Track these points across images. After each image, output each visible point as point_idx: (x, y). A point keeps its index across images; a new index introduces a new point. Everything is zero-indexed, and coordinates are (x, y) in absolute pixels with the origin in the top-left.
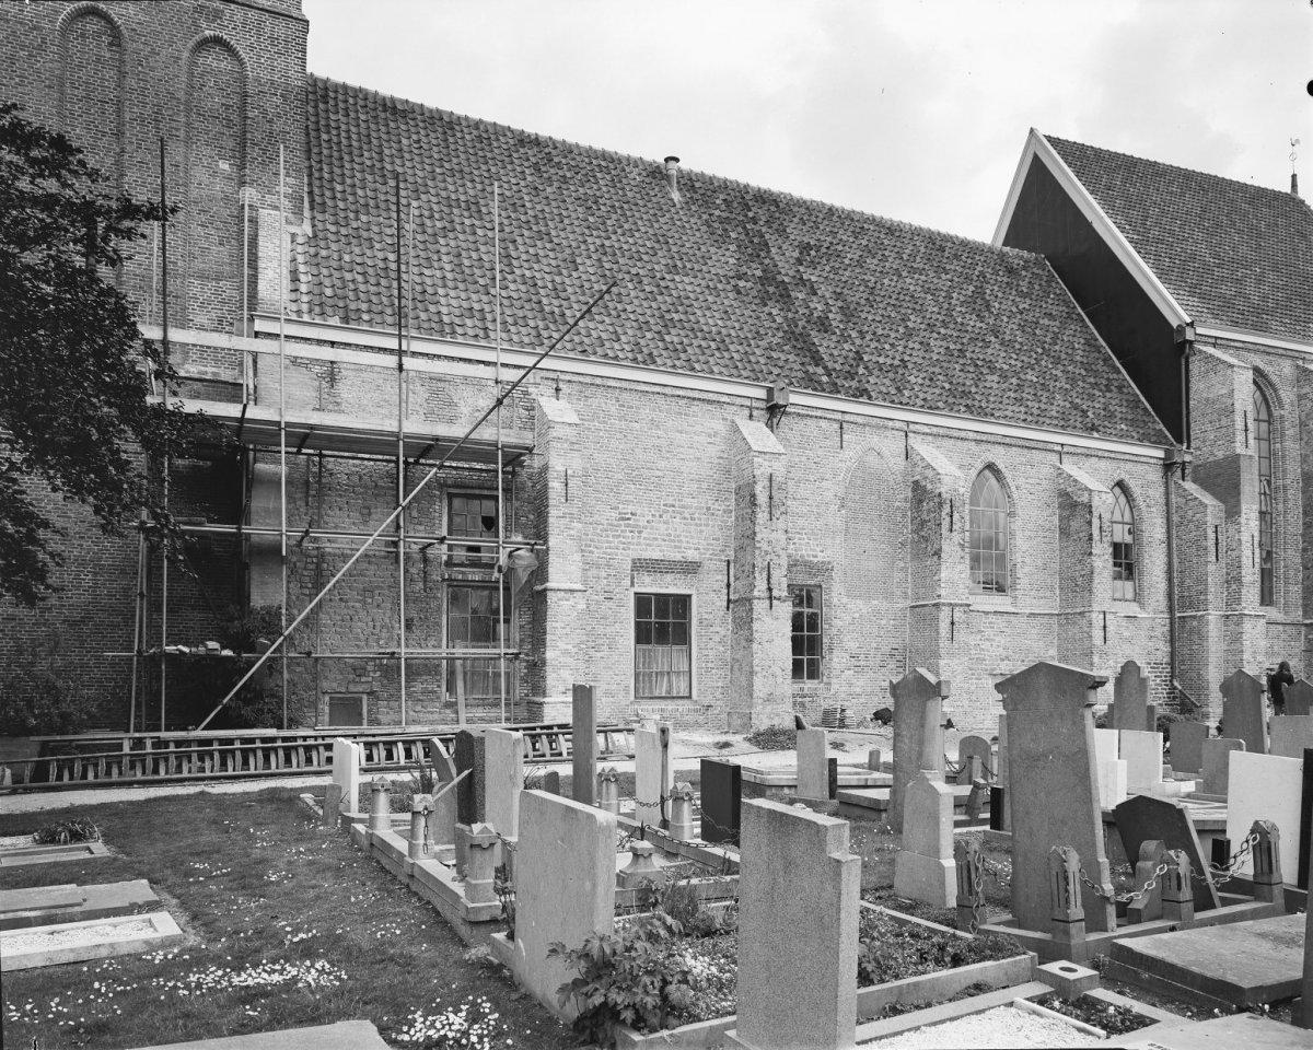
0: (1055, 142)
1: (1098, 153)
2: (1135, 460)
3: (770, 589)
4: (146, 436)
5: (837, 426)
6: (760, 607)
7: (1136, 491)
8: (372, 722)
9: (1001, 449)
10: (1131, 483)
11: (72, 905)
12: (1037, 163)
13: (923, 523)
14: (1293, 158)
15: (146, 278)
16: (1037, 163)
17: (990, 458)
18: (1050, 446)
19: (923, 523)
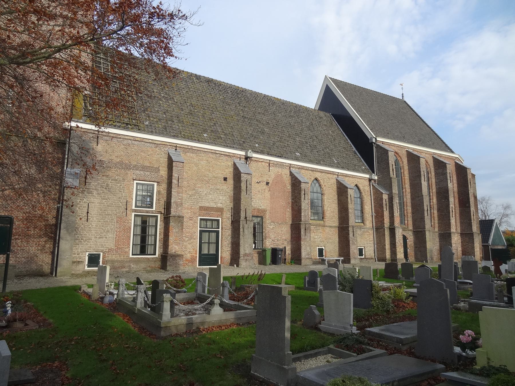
5: (268, 165)
7: (361, 188)
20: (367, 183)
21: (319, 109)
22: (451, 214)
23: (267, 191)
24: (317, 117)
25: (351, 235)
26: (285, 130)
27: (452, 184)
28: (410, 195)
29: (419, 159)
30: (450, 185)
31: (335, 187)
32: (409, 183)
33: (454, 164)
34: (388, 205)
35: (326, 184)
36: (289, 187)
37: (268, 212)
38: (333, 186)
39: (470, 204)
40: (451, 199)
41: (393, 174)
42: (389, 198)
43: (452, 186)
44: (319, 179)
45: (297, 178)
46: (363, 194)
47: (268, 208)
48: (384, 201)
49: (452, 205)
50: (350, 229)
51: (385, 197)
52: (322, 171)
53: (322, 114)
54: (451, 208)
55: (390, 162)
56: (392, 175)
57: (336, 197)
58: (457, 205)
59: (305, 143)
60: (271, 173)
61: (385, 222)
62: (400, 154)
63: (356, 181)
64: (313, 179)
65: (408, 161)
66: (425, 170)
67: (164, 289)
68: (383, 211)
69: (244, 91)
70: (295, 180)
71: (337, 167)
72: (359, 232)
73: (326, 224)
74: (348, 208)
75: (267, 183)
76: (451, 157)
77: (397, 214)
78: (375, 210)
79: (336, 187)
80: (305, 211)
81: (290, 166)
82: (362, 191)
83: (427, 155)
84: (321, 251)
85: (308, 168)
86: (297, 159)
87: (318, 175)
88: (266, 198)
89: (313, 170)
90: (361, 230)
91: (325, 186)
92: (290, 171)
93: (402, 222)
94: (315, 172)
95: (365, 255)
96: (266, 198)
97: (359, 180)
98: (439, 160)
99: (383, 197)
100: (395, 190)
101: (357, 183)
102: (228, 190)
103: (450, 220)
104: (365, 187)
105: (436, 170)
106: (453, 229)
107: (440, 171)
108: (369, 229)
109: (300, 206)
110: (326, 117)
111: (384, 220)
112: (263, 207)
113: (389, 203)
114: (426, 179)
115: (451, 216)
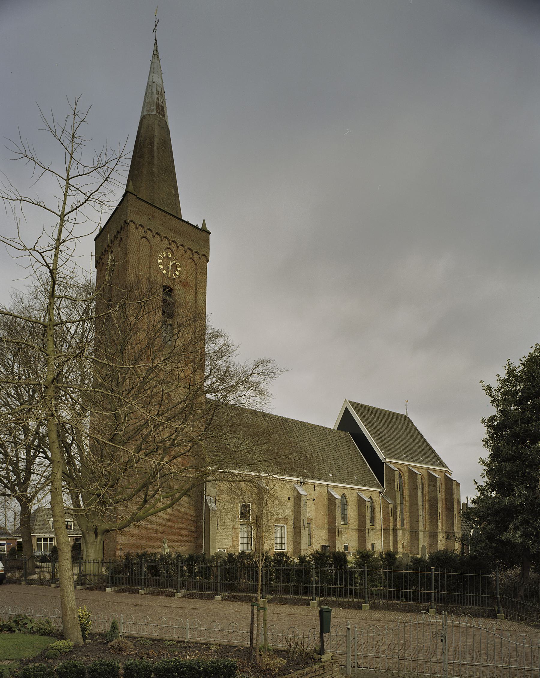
0: (351, 403)
1: (361, 405)
2: (373, 491)
3: (304, 525)
4: (517, 394)
5: (314, 486)
6: (302, 529)
7: (374, 499)
8: (483, 592)
9: (346, 490)
10: (373, 497)
11: (265, 624)
12: (347, 410)
13: (332, 509)
14: (406, 405)
15: (12, 558)
16: (347, 410)
17: (344, 492)
18: (356, 489)
19: (332, 509)
20: (378, 495)
21: (339, 428)
22: (438, 517)
23: (313, 505)
24: (339, 437)
25: (367, 534)
26: (319, 454)
27: (440, 494)
28: (408, 503)
29: (417, 476)
30: (439, 495)
31: (356, 500)
32: (408, 494)
33: (444, 476)
34: (392, 512)
35: (350, 497)
36: (326, 502)
37: (314, 519)
38: (355, 498)
39: (453, 509)
40: (439, 506)
41: (397, 489)
42: (393, 507)
43: (441, 495)
44: (346, 494)
45: (332, 495)
46: (375, 504)
47: (314, 517)
48: (390, 509)
49: (439, 511)
50: (367, 531)
51: (391, 506)
52: (347, 488)
53: (342, 433)
54: (438, 513)
55: (395, 479)
56: (396, 489)
57: (356, 508)
58: (444, 510)
59: (334, 464)
60: (316, 492)
61: (390, 525)
62: (402, 471)
63: (370, 494)
64: (342, 494)
65: (409, 476)
66: (421, 484)
67: (21, 540)
68: (389, 517)
69: (287, 420)
70: (331, 497)
71: (357, 484)
72: (371, 533)
73: (350, 527)
74: (365, 516)
75: (314, 500)
76: (441, 471)
77: (399, 519)
78: (383, 516)
79: (356, 500)
80: (338, 519)
81: (327, 486)
82: (374, 501)
83: (423, 470)
84: (346, 547)
85: (338, 487)
86: (331, 481)
87: (345, 491)
88: (313, 510)
89: (342, 488)
90: (373, 531)
91: (349, 499)
92: (327, 490)
93: (402, 525)
94: (343, 489)
95: (375, 550)
96: (313, 510)
97: (372, 493)
98: (432, 474)
99: (390, 506)
100: (398, 501)
101: (371, 495)
102: (290, 506)
103: (437, 522)
104: (376, 498)
105: (429, 482)
106: (439, 530)
107: (432, 483)
108: (379, 530)
109: (335, 516)
110: (347, 436)
111: (389, 523)
112: (311, 517)
113: (394, 511)
114: (421, 491)
115: (438, 519)
